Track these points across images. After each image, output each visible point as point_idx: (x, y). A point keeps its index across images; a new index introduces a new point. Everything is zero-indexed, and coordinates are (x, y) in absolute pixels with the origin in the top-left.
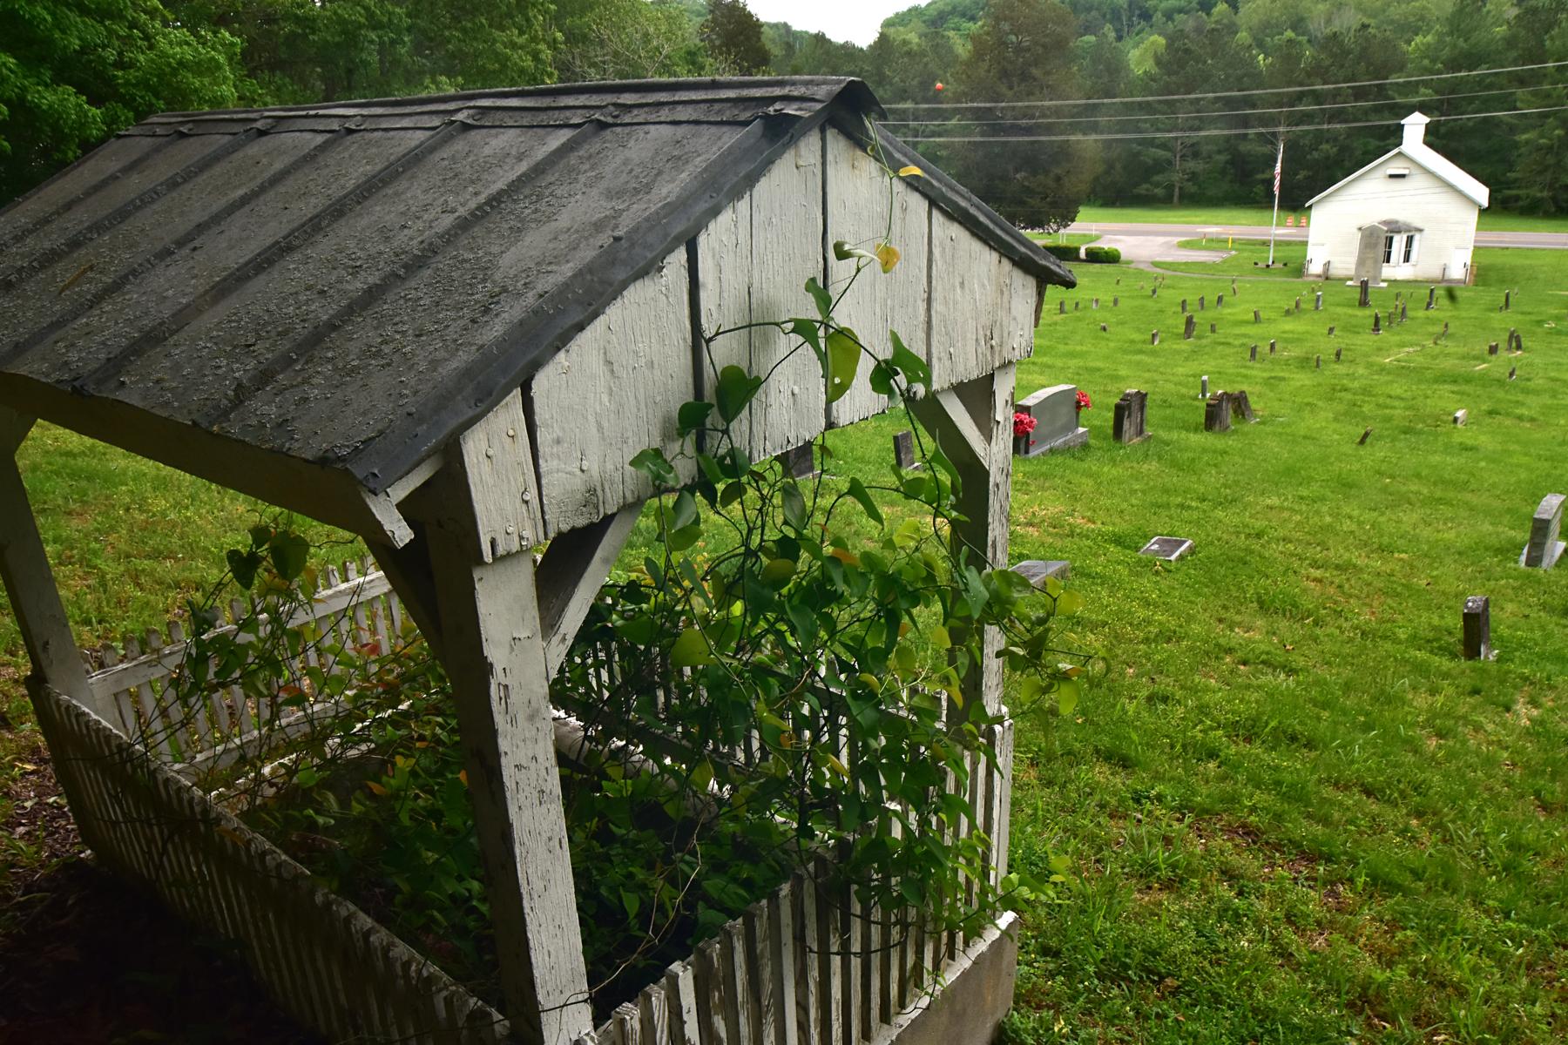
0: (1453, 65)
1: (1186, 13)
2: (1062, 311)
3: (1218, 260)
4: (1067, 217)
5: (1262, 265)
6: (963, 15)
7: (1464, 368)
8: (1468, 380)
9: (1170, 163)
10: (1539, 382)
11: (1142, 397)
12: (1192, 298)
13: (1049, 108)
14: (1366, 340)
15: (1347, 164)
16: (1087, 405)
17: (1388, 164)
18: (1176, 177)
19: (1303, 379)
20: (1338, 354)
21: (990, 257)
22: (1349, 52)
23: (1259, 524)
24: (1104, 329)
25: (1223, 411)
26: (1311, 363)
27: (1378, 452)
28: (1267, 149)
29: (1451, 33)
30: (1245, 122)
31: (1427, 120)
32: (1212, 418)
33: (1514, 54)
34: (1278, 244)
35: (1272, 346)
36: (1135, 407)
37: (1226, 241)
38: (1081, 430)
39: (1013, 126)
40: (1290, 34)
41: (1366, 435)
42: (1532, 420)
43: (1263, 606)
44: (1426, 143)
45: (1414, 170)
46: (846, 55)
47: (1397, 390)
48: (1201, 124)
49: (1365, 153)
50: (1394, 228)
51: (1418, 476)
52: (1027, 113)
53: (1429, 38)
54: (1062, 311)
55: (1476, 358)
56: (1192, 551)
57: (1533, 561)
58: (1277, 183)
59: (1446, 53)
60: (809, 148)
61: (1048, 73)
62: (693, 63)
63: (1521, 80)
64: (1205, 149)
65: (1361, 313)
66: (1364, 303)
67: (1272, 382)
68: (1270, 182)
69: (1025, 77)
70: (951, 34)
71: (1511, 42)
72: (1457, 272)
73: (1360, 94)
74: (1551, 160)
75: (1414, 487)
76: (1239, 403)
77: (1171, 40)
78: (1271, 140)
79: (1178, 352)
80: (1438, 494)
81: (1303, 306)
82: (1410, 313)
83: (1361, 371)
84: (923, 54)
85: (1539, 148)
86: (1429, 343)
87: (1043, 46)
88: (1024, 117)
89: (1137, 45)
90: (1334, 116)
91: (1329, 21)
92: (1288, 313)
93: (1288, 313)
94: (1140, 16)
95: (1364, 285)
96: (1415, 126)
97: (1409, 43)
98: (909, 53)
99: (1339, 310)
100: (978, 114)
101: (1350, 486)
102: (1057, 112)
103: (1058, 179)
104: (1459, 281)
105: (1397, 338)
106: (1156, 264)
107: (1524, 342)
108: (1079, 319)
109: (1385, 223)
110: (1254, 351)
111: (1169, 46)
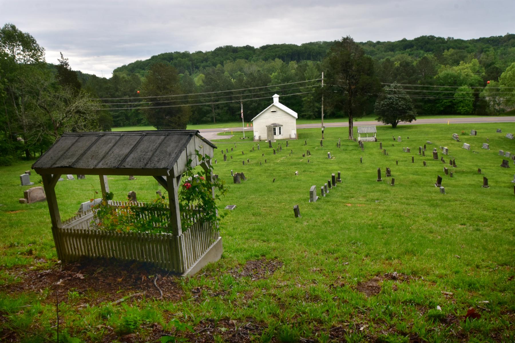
0: (284, 81)
3: (230, 138)
5: (242, 138)
6: (141, 68)
8: (299, 164)
9: (211, 111)
10: (315, 163)
12: (224, 150)
14: (273, 156)
15: (261, 108)
18: (213, 115)
19: (257, 168)
20: (266, 161)
21: (208, 146)
22: (256, 78)
23: (251, 201)
25: (238, 178)
26: (259, 164)
27: (277, 184)
28: (238, 105)
30: (231, 99)
32: (236, 180)
33: (297, 77)
34: (245, 132)
35: (248, 161)
37: (231, 132)
39: (163, 103)
40: (239, 73)
41: (274, 180)
42: (314, 172)
43: (253, 215)
44: (279, 102)
45: (278, 110)
46: (137, 67)
47: (281, 168)
49: (265, 105)
50: (275, 125)
51: (287, 187)
52: (167, 99)
53: (276, 74)
55: (300, 158)
56: (236, 207)
57: (312, 201)
58: (242, 115)
59: (281, 77)
60: (193, 137)
61: (172, 87)
63: (301, 85)
64: (221, 106)
66: (270, 147)
67: (249, 170)
68: (241, 114)
69: (165, 88)
70: (137, 74)
71: (296, 75)
72: (293, 136)
74: (312, 105)
75: (286, 190)
76: (242, 176)
78: (239, 103)
79: (223, 165)
80: (291, 191)
81: (255, 149)
82: (282, 148)
83: (272, 165)
84: (130, 81)
85: (308, 102)
86: (288, 156)
87: (170, 79)
88: (166, 100)
89: (196, 77)
90: (255, 96)
91: (249, 69)
92: (251, 151)
93: (251, 151)
94: (196, 68)
95: (270, 142)
96: (276, 98)
97: (271, 74)
98: (125, 81)
99: (264, 149)
100: (151, 100)
101: (271, 191)
102: (176, 98)
103: (179, 118)
109: (273, 124)
110: (243, 162)
111: (206, 77)
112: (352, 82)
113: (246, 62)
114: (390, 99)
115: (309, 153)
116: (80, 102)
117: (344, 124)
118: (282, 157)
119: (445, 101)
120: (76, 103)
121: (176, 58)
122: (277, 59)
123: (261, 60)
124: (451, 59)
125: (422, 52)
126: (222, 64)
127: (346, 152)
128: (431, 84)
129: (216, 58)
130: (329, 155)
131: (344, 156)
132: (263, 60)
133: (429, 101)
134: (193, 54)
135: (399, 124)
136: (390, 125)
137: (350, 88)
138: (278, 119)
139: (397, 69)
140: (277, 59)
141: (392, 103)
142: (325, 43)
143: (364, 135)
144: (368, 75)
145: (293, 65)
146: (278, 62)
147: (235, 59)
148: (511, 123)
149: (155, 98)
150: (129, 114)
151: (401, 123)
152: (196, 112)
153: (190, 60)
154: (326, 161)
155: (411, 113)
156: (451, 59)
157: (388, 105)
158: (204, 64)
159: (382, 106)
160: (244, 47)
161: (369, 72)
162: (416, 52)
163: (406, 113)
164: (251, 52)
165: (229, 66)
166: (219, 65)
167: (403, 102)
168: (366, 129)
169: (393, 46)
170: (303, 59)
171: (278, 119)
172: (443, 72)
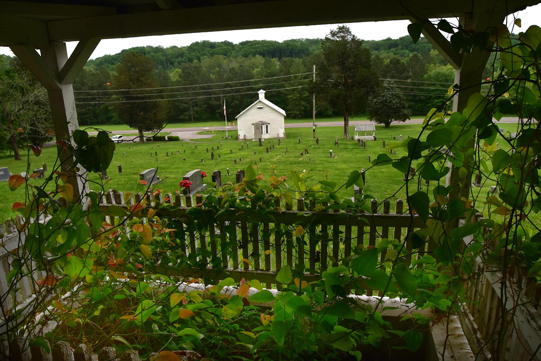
1: (185, 63)
2: (212, 158)
3: (211, 137)
4: (160, 127)
5: (224, 138)
6: (109, 63)
7: (296, 160)
10: (317, 161)
11: (219, 172)
13: (148, 91)
14: (265, 155)
16: (205, 176)
17: (255, 105)
18: (191, 113)
20: (260, 160)
22: (238, 73)
24: (184, 159)
29: (265, 68)
31: (265, 92)
34: (228, 131)
36: (218, 176)
37: (212, 131)
38: (204, 185)
40: (217, 69)
46: (106, 61)
48: (197, 94)
49: (247, 103)
52: (141, 92)
54: (168, 156)
55: (298, 157)
62: (8, 75)
63: (285, 80)
65: (261, 148)
69: (138, 80)
72: (282, 135)
73: (243, 84)
74: (297, 103)
77: (183, 70)
79: (212, 164)
81: (244, 147)
84: (98, 75)
85: (294, 100)
86: (284, 154)
91: (228, 65)
92: (240, 149)
93: (240, 149)
94: (170, 63)
96: (262, 94)
98: (93, 74)
99: (254, 148)
100: (123, 93)
102: (151, 92)
103: (155, 114)
104: (282, 138)
105: (274, 154)
106: (191, 140)
107: (309, 152)
108: (174, 158)
111: (183, 72)
112: (348, 76)
113: (224, 58)
114: (383, 96)
115: (307, 151)
116: (40, 92)
117: (339, 123)
118: (277, 155)
119: (437, 101)
120: (35, 92)
121: (149, 53)
122: (257, 56)
123: (240, 56)
124: (438, 59)
125: (407, 51)
126: (199, 59)
127: (347, 151)
128: (423, 84)
129: (193, 54)
130: (331, 153)
131: (346, 155)
132: (243, 56)
133: (420, 101)
134: (167, 48)
135: (392, 124)
136: (383, 125)
137: (346, 82)
138: (264, 118)
139: (387, 66)
140: (257, 56)
141: (386, 101)
142: (307, 40)
143: (362, 133)
144: (366, 68)
145: (276, 63)
146: (259, 59)
147: (212, 55)
148: (505, 124)
149: (128, 91)
150: (98, 112)
151: (394, 123)
153: (164, 55)
154: (329, 159)
155: (406, 112)
156: (438, 59)
157: (381, 103)
158: (180, 59)
159: (375, 105)
160: (222, 42)
161: (366, 65)
162: (401, 52)
163: (400, 111)
164: (230, 48)
165: (206, 62)
166: (195, 61)
167: (397, 100)
168: (364, 127)
169: (377, 45)
170: (285, 56)
171: (264, 118)
172: (434, 71)
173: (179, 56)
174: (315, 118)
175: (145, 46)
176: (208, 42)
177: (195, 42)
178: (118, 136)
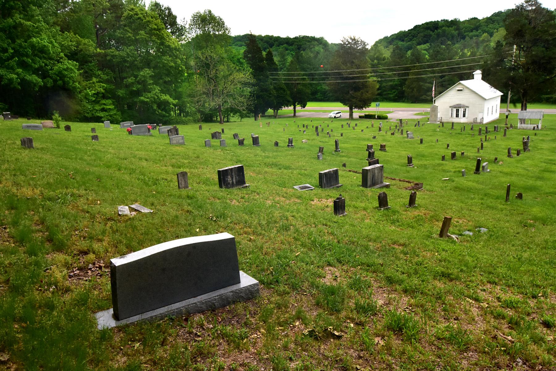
152: (415, 90)
171: (478, 99)
173: (474, 29)
174: (510, 102)
175: (440, 20)
176: (268, 36)
177: (497, 11)
178: (336, 112)
